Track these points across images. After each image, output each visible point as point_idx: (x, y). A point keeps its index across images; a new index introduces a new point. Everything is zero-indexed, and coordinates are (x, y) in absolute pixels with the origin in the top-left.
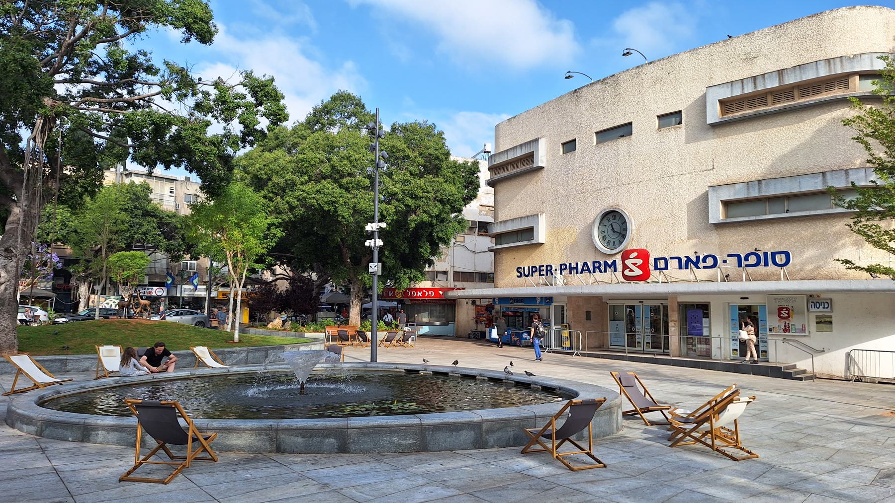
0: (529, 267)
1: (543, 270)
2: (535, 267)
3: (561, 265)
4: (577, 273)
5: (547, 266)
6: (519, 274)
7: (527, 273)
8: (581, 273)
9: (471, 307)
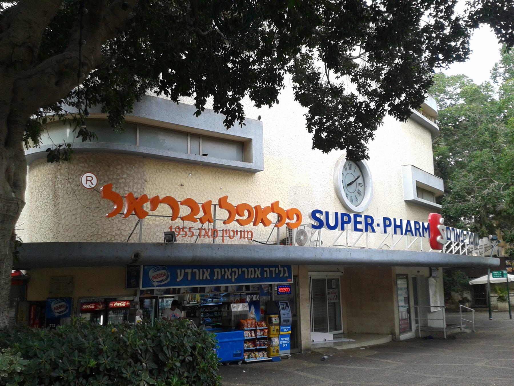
0: (336, 214)
1: (360, 223)
2: (389, 219)
3: (385, 219)
4: (402, 234)
5: (366, 217)
6: (316, 224)
7: (332, 223)
8: (406, 234)
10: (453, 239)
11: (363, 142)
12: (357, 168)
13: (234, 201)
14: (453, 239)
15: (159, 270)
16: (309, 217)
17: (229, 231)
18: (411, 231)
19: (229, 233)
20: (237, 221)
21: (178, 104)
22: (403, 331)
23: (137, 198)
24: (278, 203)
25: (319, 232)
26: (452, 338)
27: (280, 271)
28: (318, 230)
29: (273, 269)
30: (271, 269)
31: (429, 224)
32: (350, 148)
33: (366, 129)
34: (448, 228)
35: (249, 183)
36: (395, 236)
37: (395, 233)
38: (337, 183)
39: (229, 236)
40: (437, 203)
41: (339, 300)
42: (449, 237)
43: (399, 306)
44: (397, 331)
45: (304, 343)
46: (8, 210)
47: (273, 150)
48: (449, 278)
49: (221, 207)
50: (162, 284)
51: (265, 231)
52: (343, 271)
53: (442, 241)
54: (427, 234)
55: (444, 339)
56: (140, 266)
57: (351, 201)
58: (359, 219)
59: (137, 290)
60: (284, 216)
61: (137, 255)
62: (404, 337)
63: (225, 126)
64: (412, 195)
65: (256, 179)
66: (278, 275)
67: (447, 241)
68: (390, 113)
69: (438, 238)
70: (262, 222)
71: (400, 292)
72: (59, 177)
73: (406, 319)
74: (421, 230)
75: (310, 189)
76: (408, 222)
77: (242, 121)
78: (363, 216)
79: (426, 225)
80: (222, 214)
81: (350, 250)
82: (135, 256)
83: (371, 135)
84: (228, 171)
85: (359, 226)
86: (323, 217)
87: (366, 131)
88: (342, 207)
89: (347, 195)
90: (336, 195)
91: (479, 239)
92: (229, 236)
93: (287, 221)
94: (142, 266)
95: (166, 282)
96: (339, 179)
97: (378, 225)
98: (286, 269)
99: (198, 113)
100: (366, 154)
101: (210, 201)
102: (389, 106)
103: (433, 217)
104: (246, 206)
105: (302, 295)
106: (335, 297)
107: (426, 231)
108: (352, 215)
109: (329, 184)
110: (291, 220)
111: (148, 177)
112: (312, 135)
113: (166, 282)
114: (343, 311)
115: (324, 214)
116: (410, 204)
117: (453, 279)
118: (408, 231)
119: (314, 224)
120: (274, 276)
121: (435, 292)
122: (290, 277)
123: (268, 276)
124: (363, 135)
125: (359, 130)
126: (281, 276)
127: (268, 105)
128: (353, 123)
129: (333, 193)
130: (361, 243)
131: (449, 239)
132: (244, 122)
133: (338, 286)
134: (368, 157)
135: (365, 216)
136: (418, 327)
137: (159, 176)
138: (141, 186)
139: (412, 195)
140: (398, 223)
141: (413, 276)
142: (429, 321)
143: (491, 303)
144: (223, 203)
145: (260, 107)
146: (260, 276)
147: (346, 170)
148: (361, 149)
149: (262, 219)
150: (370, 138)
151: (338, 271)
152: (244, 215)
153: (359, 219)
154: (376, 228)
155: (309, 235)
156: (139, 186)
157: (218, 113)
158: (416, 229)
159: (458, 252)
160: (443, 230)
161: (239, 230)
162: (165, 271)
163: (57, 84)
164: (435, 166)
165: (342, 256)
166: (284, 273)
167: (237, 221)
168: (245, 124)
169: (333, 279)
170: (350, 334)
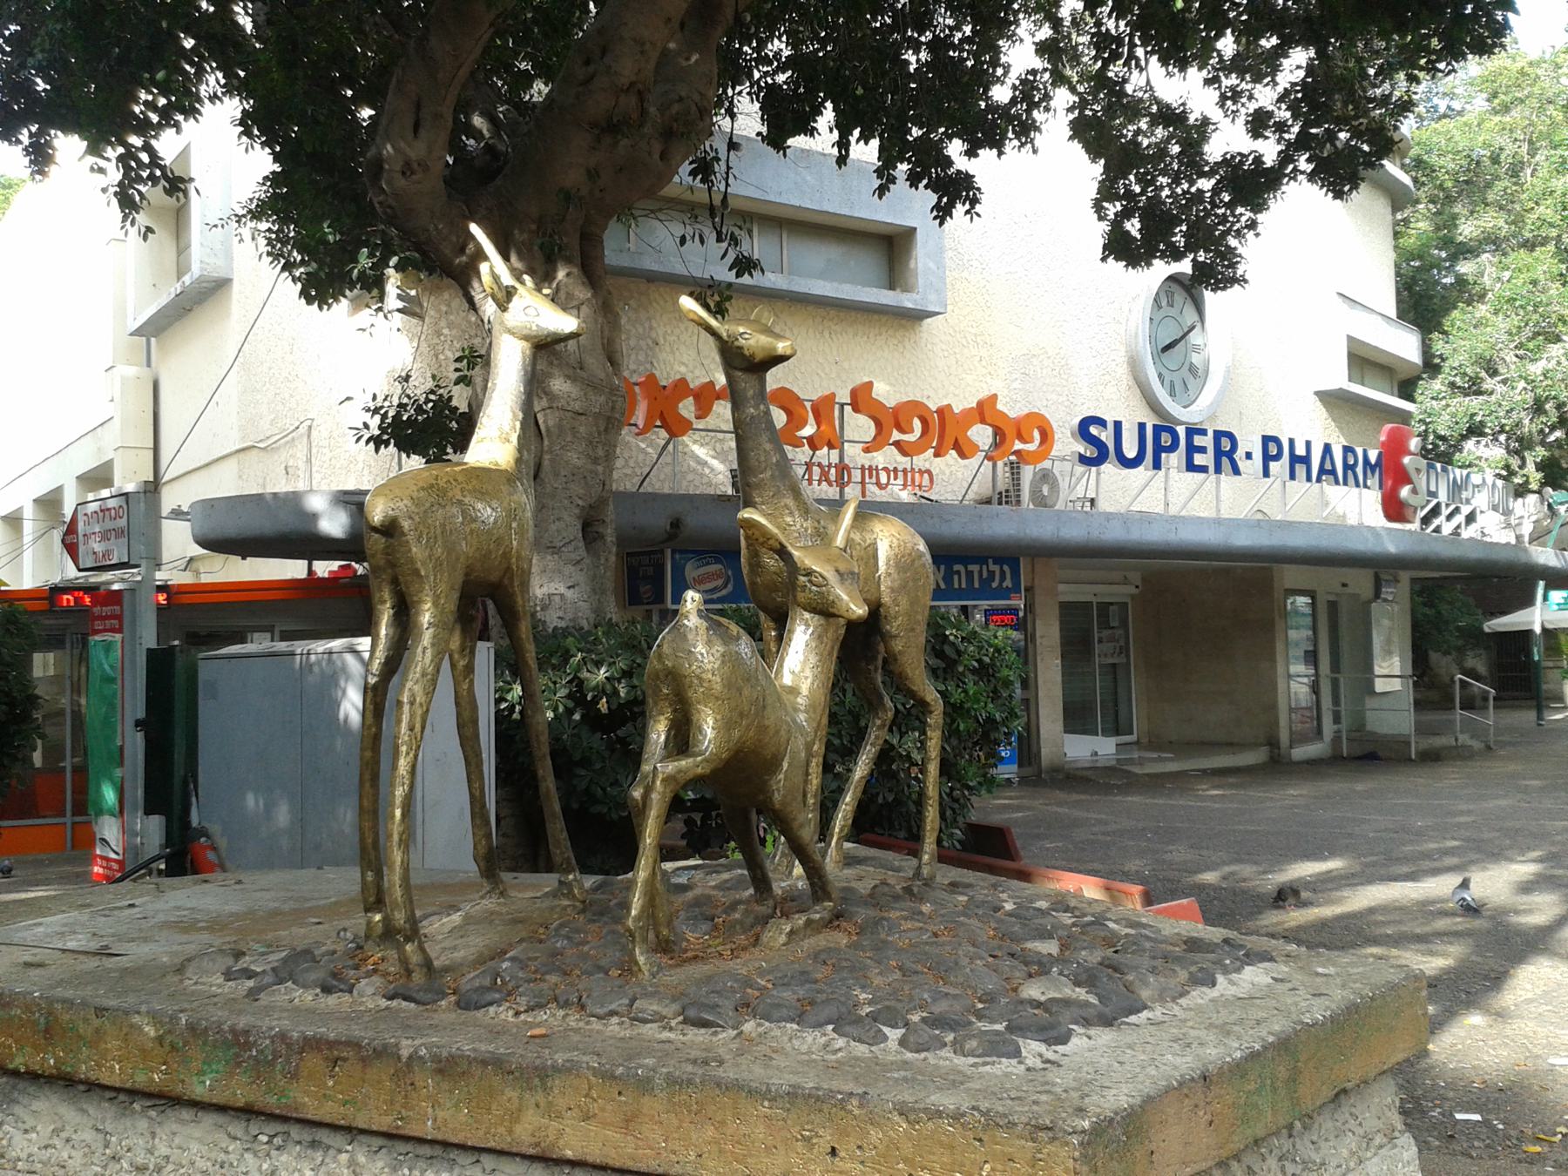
0: (1142, 426)
1: (1203, 450)
2: (1276, 440)
3: (1266, 440)
4: (1309, 479)
5: (1218, 435)
6: (1090, 452)
7: (1130, 451)
8: (1319, 480)
9: (1278, 79)
10: (1443, 497)
11: (1233, 242)
12: (1189, 300)
13: (886, 393)
14: (1443, 497)
15: (708, 564)
16: (1073, 434)
17: (877, 469)
18: (1333, 472)
19: (878, 474)
20: (897, 444)
21: (785, 155)
22: (1298, 739)
23: (665, 387)
24: (994, 398)
25: (1098, 474)
26: (1431, 757)
27: (992, 574)
28: (1094, 469)
29: (974, 568)
30: (970, 567)
31: (1380, 454)
32: (1201, 259)
33: (1240, 210)
34: (1431, 467)
35: (908, 346)
36: (1290, 484)
37: (1292, 476)
38: (1137, 343)
39: (878, 484)
40: (1401, 397)
41: (1128, 656)
42: (1433, 488)
43: (1289, 676)
44: (1284, 737)
45: (1047, 753)
46: (613, 408)
47: (966, 257)
48: (1427, 610)
49: (856, 410)
50: (715, 596)
51: (947, 472)
52: (1139, 584)
53: (1413, 501)
54: (1373, 481)
55: (1411, 760)
56: (662, 552)
57: (1172, 394)
58: (1198, 441)
59: (651, 611)
60: (1010, 432)
61: (676, 524)
62: (1299, 753)
63: (935, 218)
64: (1338, 377)
65: (924, 335)
66: (987, 583)
67: (1428, 502)
68: (1311, 177)
69: (1405, 492)
70: (957, 447)
71: (1293, 634)
72: (446, 331)
73: (1309, 709)
74: (1359, 470)
75: (1063, 362)
76: (1327, 449)
77: (972, 207)
78: (1210, 433)
79: (1373, 456)
80: (859, 427)
81: (1177, 520)
82: (672, 524)
83: (1252, 225)
84: (853, 314)
85: (1199, 459)
86: (1106, 436)
87: (1241, 215)
88: (1148, 410)
89: (1160, 375)
90: (1131, 378)
91: (1515, 500)
92: (878, 484)
93: (1018, 446)
94: (668, 553)
95: (724, 592)
96: (1140, 334)
97: (1249, 456)
98: (1006, 568)
99: (882, 191)
100: (1240, 272)
101: (833, 395)
102: (1309, 161)
103: (1391, 434)
104: (915, 408)
105: (1042, 637)
106: (1118, 650)
107: (1373, 473)
108: (1181, 430)
109: (1113, 347)
110: (1025, 442)
111: (661, 332)
112: (1105, 227)
113: (724, 592)
114: (1136, 685)
115: (1111, 426)
116: (1334, 400)
117: (1439, 613)
118: (1327, 471)
119: (1082, 452)
120: (977, 585)
121: (1389, 641)
122: (1016, 588)
123: (964, 586)
124: (1233, 224)
125: (1223, 210)
126: (995, 585)
127: (995, 151)
128: (1208, 195)
129: (1122, 371)
130: (1201, 508)
131: (1433, 494)
132: (978, 208)
133: (1124, 623)
134: (1246, 281)
135: (1215, 431)
136: (1339, 731)
137: (686, 329)
138: (647, 355)
139: (1338, 377)
140: (1300, 451)
141: (1331, 598)
142: (1368, 713)
143: (1544, 687)
144: (861, 399)
145: (976, 155)
146: (943, 586)
147: (1160, 307)
148: (1229, 260)
149: (956, 439)
150: (1252, 232)
151: (1126, 581)
152: (912, 431)
153: (1198, 441)
154: (1243, 465)
155: (1063, 484)
156: (641, 357)
157: (917, 188)
158: (1346, 467)
159: (1456, 532)
160: (1418, 470)
161: (900, 468)
162: (720, 566)
163: (663, 156)
164: (1398, 293)
165: (1154, 535)
166: (1003, 578)
167: (897, 444)
168: (978, 215)
169: (1112, 604)
170: (1154, 743)
